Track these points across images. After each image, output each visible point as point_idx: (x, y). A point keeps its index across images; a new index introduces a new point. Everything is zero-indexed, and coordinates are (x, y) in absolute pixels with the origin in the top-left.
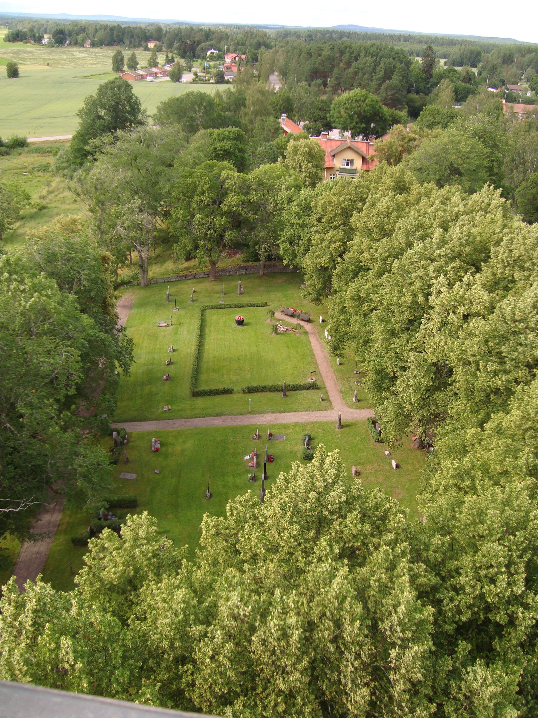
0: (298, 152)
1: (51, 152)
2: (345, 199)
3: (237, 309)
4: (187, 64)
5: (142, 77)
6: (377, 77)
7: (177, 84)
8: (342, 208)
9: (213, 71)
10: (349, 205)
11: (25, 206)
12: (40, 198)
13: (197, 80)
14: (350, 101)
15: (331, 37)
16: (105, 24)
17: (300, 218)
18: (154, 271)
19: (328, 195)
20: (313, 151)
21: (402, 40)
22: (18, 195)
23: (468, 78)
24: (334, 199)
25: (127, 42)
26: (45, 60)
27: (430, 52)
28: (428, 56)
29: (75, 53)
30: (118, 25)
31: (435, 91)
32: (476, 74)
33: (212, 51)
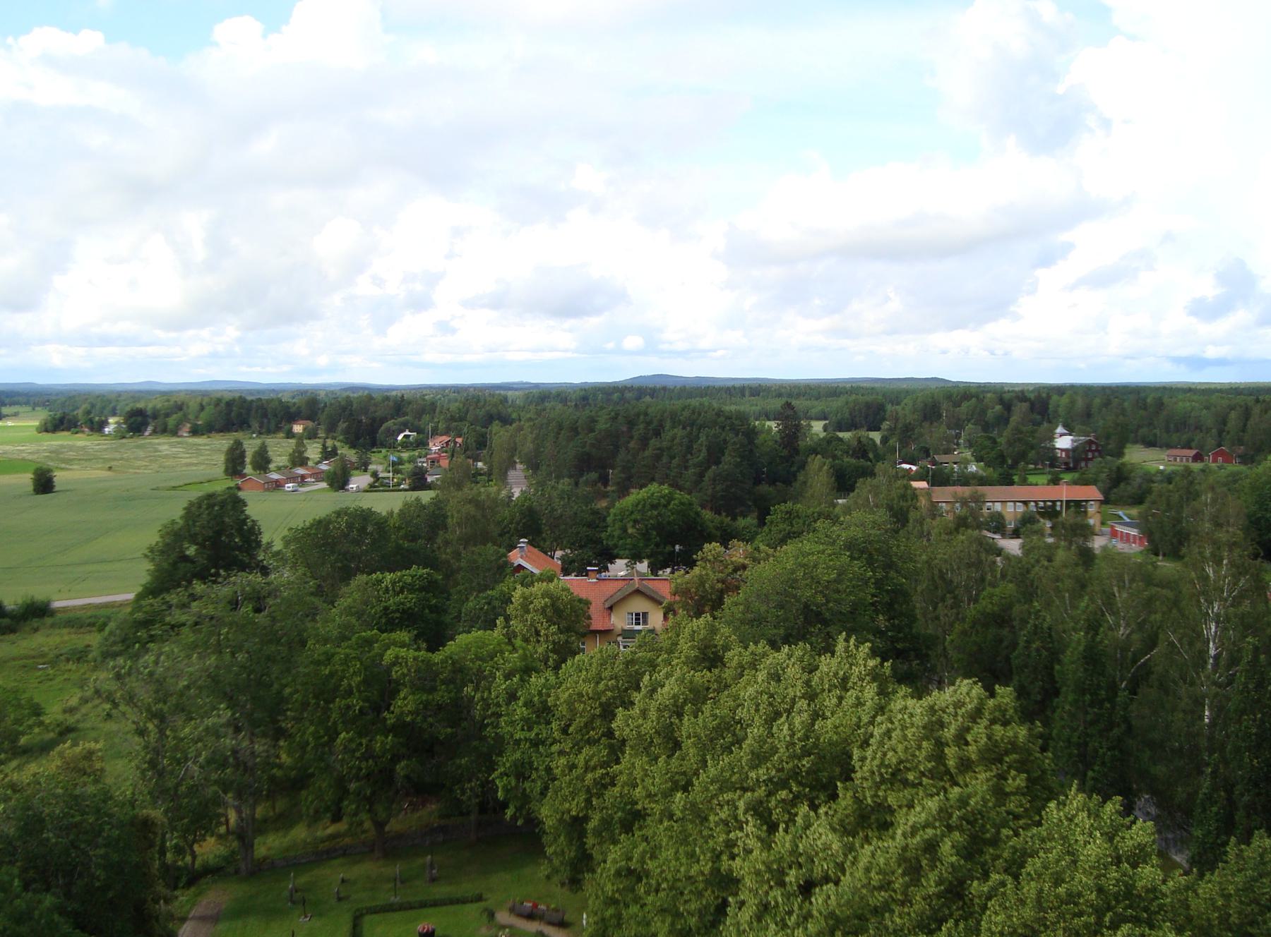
0: (531, 606)
1: (93, 625)
2: (608, 688)
3: (425, 911)
4: (360, 458)
5: (278, 485)
6: (696, 460)
7: (341, 493)
8: (601, 704)
9: (408, 467)
10: (614, 698)
11: (30, 727)
12: (65, 711)
13: (378, 484)
14: (640, 506)
15: (622, 399)
16: (219, 395)
17: (530, 729)
18: (268, 845)
19: (577, 683)
20: (559, 604)
21: (747, 393)
22: (19, 706)
23: (862, 450)
24: (587, 689)
25: (255, 425)
26: (105, 460)
27: (790, 412)
28: (787, 418)
29: (161, 448)
30: (240, 397)
31: (801, 477)
32: (878, 441)
33: (407, 433)
